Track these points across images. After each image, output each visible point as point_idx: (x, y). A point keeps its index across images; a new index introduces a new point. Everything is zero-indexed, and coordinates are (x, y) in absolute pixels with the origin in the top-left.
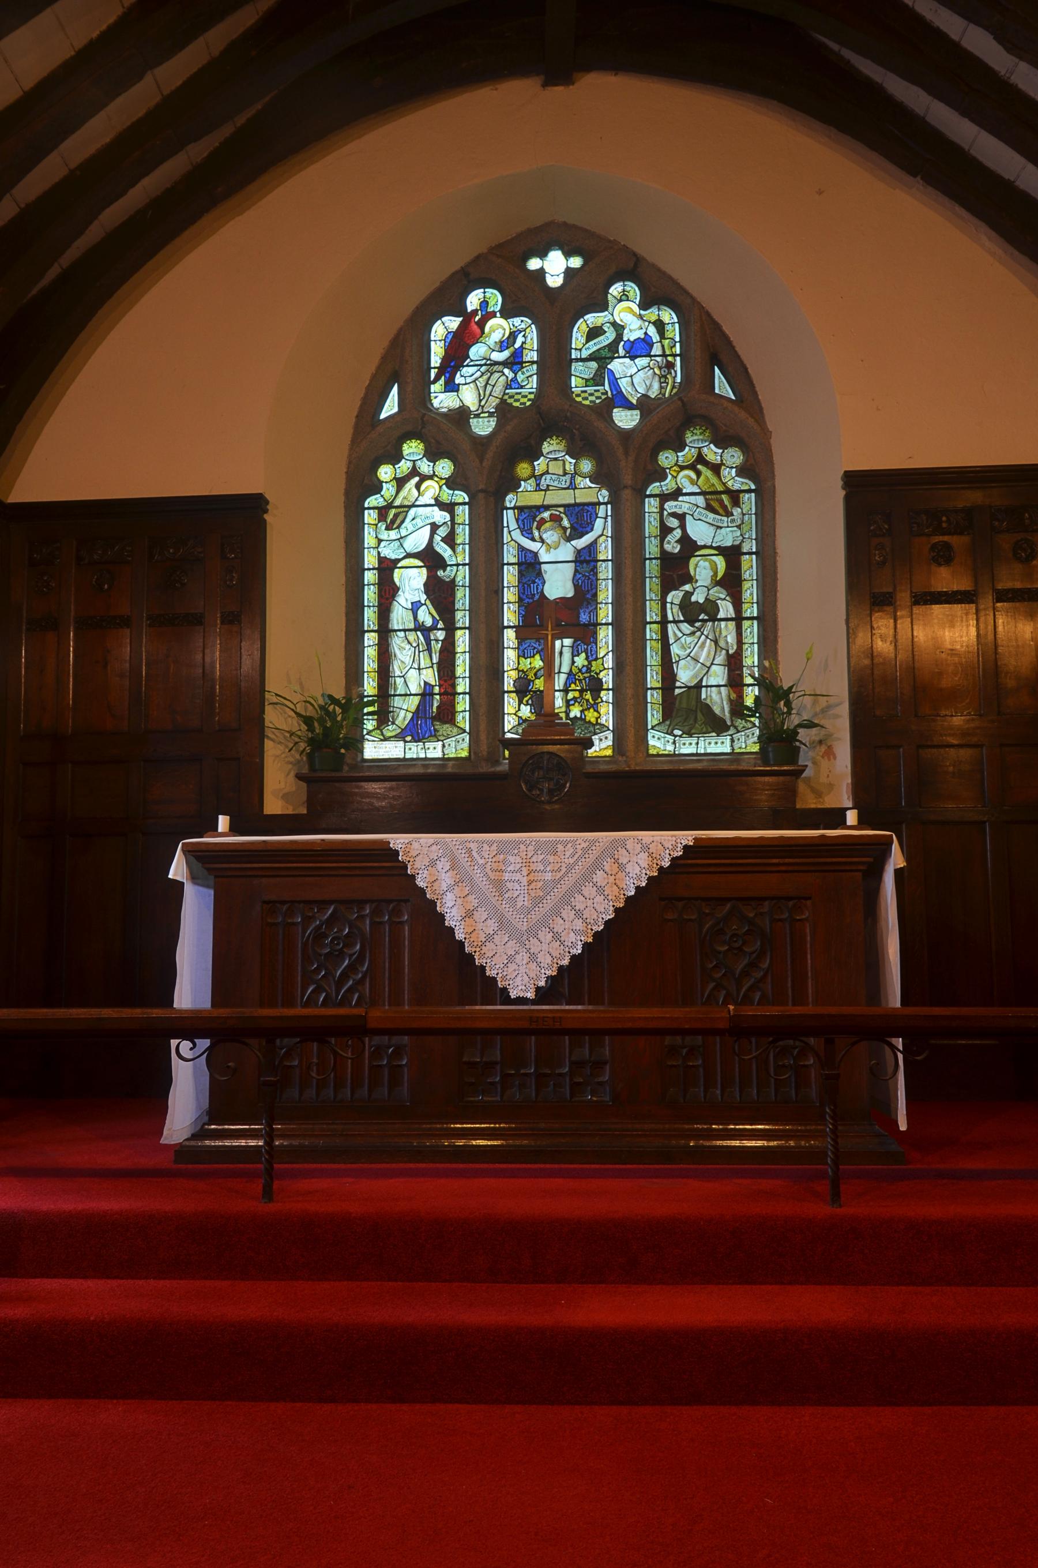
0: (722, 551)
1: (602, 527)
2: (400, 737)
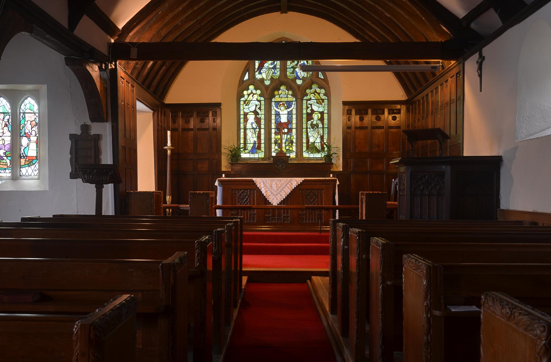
0: (320, 112)
1: (294, 107)
2: (249, 153)
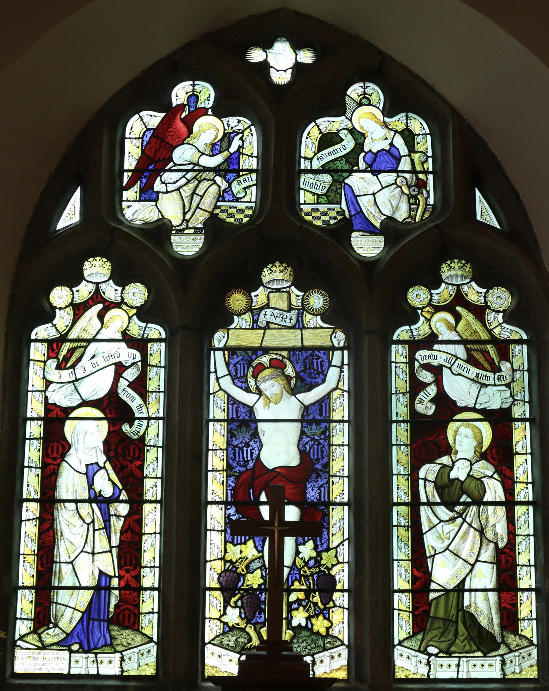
0: (488, 415)
1: (336, 379)
